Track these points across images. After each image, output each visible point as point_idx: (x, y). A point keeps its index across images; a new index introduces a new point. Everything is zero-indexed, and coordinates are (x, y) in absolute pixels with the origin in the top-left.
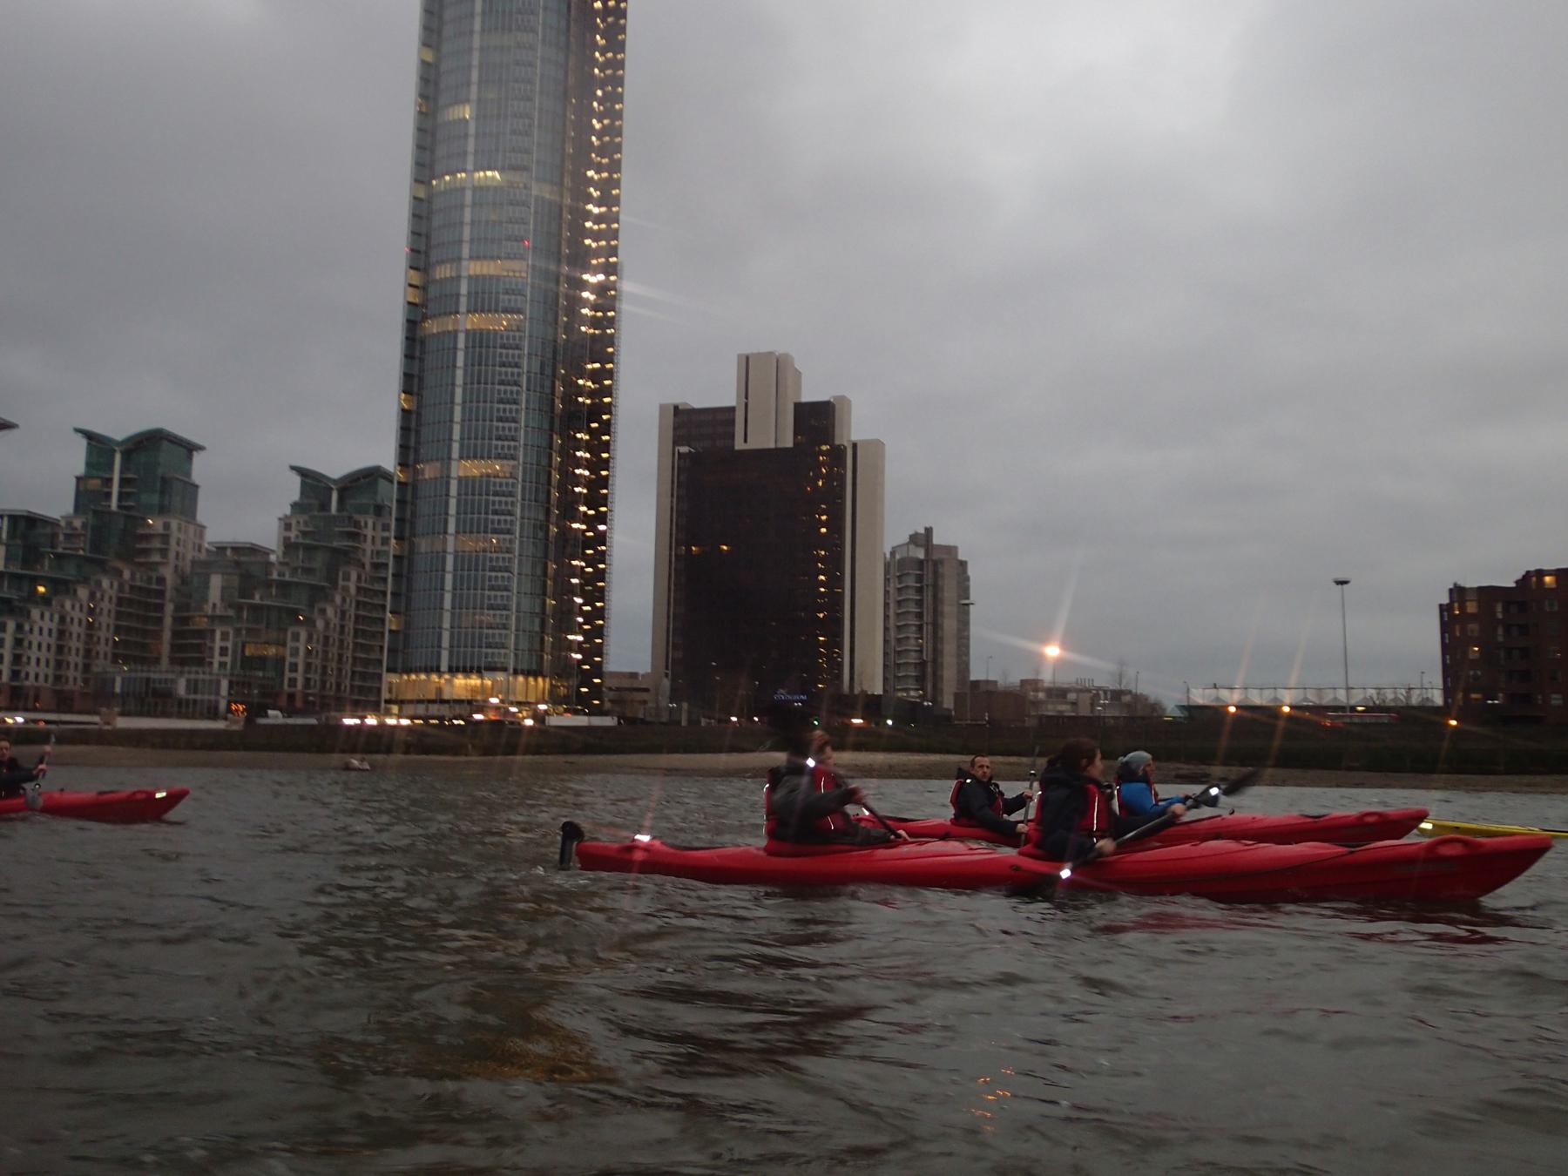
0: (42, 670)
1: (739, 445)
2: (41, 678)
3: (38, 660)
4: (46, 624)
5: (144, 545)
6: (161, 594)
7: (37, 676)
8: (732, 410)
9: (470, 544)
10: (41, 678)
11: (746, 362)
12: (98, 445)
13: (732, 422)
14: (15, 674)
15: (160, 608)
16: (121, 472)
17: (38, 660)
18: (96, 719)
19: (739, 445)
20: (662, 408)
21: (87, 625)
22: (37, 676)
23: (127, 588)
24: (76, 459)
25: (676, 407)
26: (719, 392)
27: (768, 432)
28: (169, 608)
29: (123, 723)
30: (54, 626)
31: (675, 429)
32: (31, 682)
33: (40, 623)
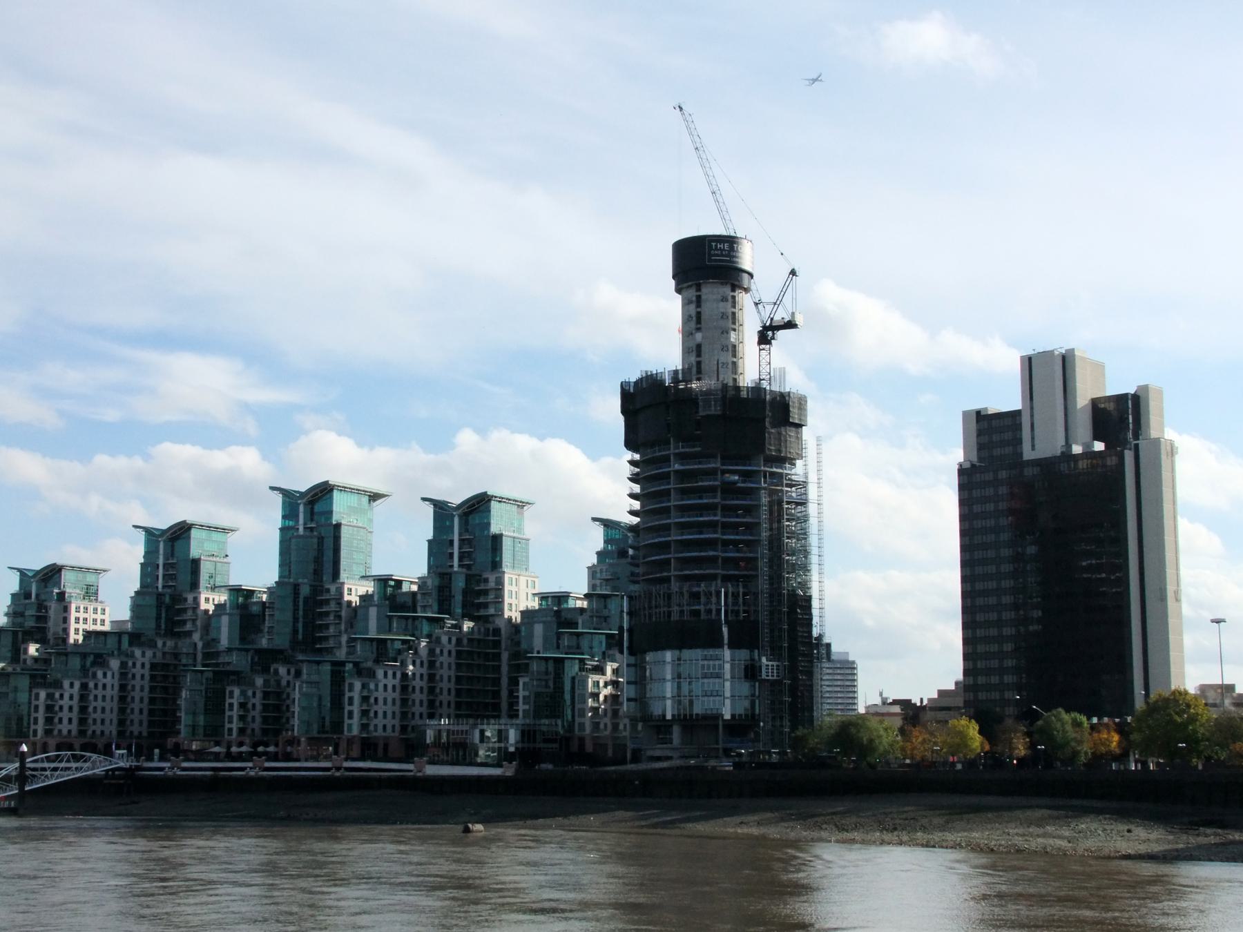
0: (390, 722)
1: (1028, 454)
2: (389, 729)
3: (385, 713)
4: (390, 682)
5: (481, 600)
6: (497, 644)
7: (385, 727)
8: (1015, 415)
9: (419, 609)
10: (389, 729)
11: (1029, 363)
12: (441, 510)
13: (1018, 427)
14: (364, 727)
15: (497, 657)
16: (460, 534)
17: (385, 713)
18: (411, 767)
19: (1028, 454)
20: (966, 415)
21: (253, 697)
22: (385, 727)
23: (465, 641)
24: (425, 528)
25: (978, 413)
26: (1006, 397)
27: (1062, 438)
28: (505, 656)
29: (431, 770)
30: (397, 682)
31: (978, 435)
32: (380, 732)
33: (384, 681)
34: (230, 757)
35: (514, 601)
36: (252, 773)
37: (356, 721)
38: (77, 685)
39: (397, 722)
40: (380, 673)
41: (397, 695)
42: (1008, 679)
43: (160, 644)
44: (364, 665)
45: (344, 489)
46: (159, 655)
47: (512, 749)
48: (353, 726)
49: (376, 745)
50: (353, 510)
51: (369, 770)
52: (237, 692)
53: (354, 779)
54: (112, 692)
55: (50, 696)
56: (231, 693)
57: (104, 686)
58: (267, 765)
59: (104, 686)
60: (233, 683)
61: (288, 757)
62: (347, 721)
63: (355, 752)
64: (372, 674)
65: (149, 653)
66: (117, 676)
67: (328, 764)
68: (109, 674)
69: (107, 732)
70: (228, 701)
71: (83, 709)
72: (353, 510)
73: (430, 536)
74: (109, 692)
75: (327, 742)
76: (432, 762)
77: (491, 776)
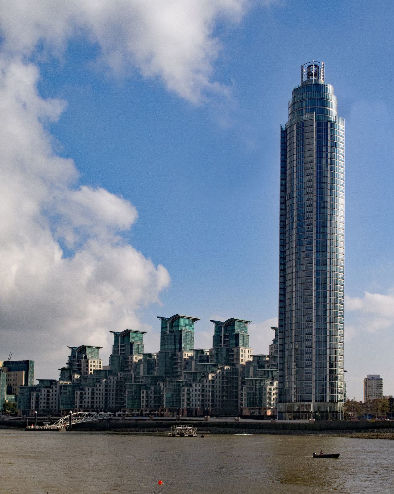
35: (243, 358)
38: (90, 389)
40: (194, 385)
43: (119, 375)
45: (183, 317)
46: (119, 378)
48: (184, 405)
49: (192, 411)
50: (186, 325)
51: (189, 420)
54: (103, 392)
55: (188, 390)
57: (100, 390)
58: (154, 418)
59: (100, 390)
63: (186, 413)
64: (191, 386)
65: (115, 378)
66: (104, 386)
68: (102, 385)
69: (101, 407)
71: (93, 398)
72: (186, 325)
74: (101, 392)
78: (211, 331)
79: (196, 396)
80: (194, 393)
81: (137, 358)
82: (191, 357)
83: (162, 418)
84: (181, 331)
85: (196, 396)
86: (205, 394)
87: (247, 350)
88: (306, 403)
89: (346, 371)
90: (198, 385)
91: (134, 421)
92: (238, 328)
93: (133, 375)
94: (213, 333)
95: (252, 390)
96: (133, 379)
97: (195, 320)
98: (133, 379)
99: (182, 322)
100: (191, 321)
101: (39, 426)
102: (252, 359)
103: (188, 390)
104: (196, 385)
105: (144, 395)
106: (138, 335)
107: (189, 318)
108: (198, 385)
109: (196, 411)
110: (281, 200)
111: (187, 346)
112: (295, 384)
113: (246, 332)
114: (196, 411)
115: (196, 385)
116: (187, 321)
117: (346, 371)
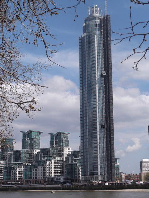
0: (41, 177)
2: (41, 178)
10: (41, 178)
14: (36, 178)
34: (11, 184)
35: (66, 153)
36: (15, 187)
37: (48, 174)
39: (42, 177)
40: (39, 167)
41: (42, 171)
42: (59, 172)
44: (36, 166)
45: (34, 132)
47: (62, 181)
49: (38, 181)
50: (36, 135)
51: (36, 186)
52: (13, 171)
53: (33, 188)
55: (36, 170)
56: (12, 171)
58: (18, 185)
60: (13, 170)
61: (22, 184)
62: (33, 177)
63: (34, 183)
64: (37, 167)
67: (29, 185)
70: (12, 173)
72: (36, 135)
73: (50, 140)
75: (29, 181)
76: (47, 184)
77: (55, 187)
78: (49, 138)
79: (40, 173)
80: (39, 171)
81: (36, 151)
82: (38, 152)
83: (22, 185)
84: (33, 138)
85: (40, 173)
86: (51, 169)
87: (68, 148)
88: (95, 176)
89: (131, 7)
90: (41, 167)
91: (7, 187)
92: (62, 137)
93: (8, 162)
94: (80, 144)
95: (69, 169)
96: (8, 164)
97: (40, 133)
98: (8, 164)
99: (33, 134)
100: (38, 134)
101: (131, 146)
102: (70, 153)
103: (35, 170)
104: (40, 167)
105: (13, 173)
106: (11, 141)
107: (37, 132)
108: (41, 167)
109: (40, 181)
110: (80, 56)
111: (37, 146)
112: (66, 184)
113: (67, 139)
114: (40, 181)
115: (40, 167)
116: (36, 134)
117: (131, 7)
